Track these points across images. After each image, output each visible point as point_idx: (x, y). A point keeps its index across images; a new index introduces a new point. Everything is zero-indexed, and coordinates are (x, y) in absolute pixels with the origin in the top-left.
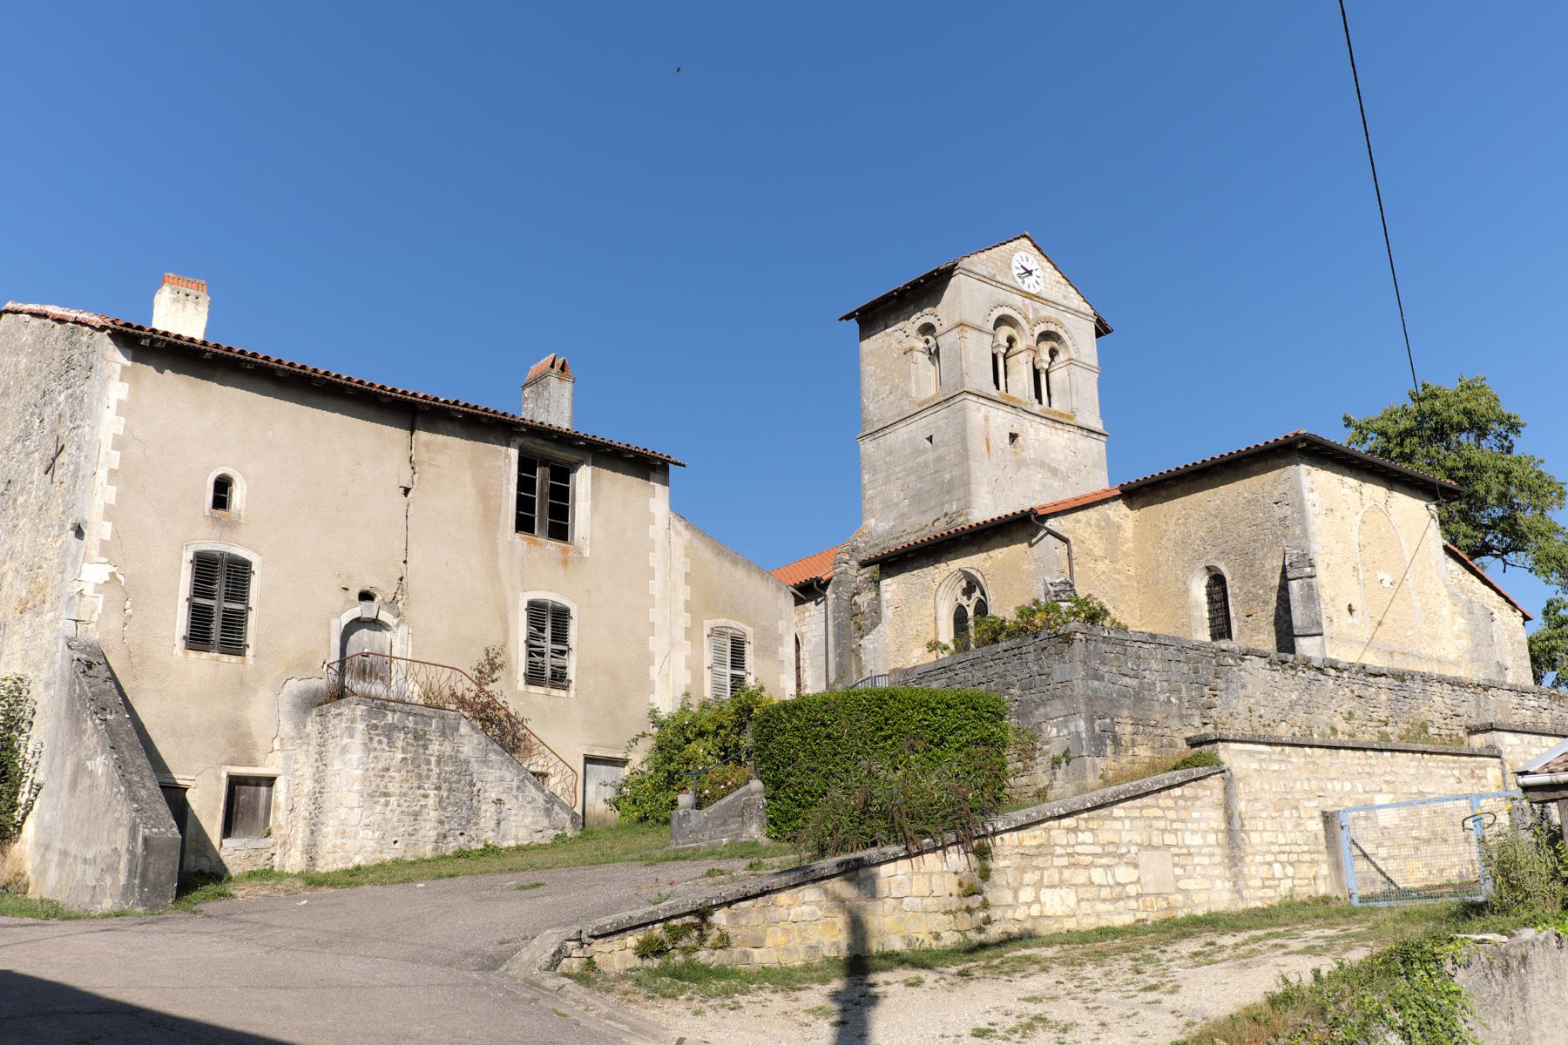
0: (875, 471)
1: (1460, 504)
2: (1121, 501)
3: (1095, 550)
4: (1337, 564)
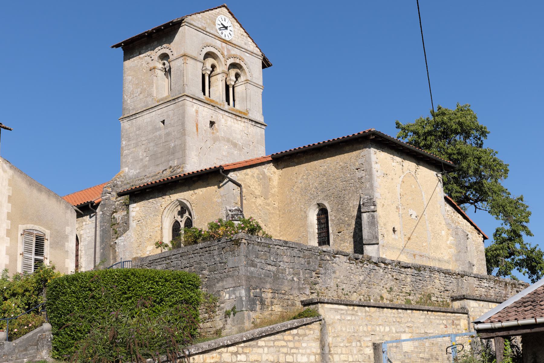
0: (129, 139)
2: (272, 164)
3: (256, 191)
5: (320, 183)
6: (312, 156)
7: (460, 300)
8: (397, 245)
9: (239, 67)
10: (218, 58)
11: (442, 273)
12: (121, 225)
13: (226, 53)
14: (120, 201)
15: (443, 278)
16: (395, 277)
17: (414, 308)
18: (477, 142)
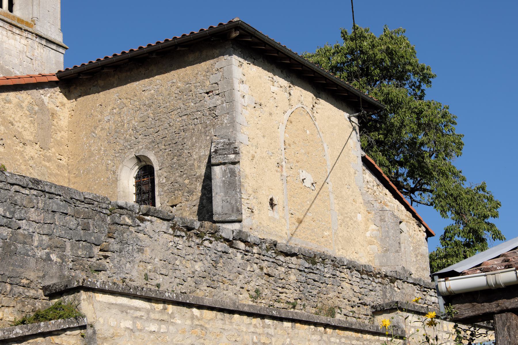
1: (379, 134)
2: (58, 89)
3: (24, 133)
4: (263, 158)
6: (129, 73)
7: (389, 313)
8: (277, 229)
11: (355, 272)
15: (358, 280)
16: (265, 271)
17: (298, 318)
18: (415, 92)
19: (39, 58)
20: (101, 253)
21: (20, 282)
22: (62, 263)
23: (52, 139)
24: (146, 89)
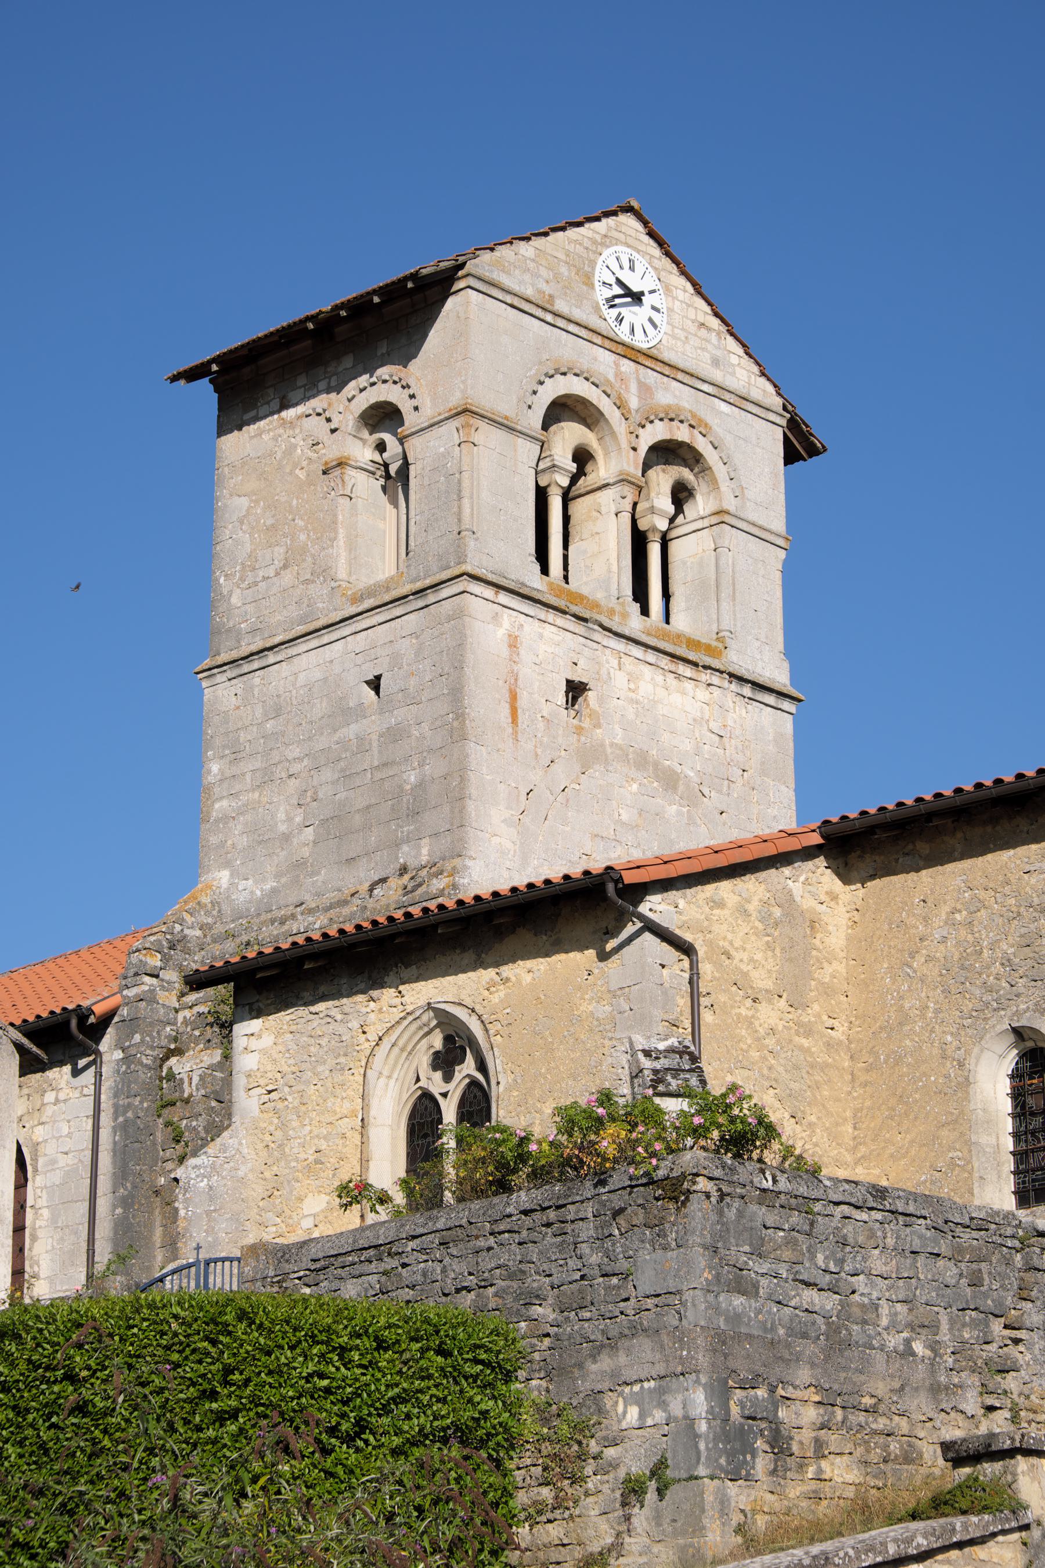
0: (236, 755)
2: (821, 862)
3: (754, 974)
5: (1024, 942)
6: (989, 829)
9: (689, 456)
10: (602, 423)
12: (200, 1108)
13: (634, 403)
14: (196, 1009)
19: (738, 732)
20: (1007, 1332)
21: (860, 1403)
22: (934, 1359)
23: (813, 983)
24: (1032, 869)
